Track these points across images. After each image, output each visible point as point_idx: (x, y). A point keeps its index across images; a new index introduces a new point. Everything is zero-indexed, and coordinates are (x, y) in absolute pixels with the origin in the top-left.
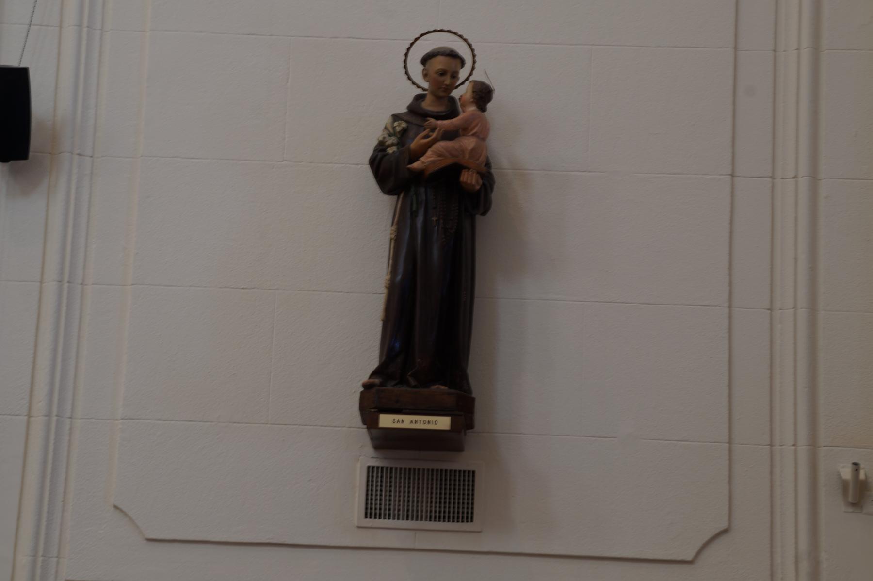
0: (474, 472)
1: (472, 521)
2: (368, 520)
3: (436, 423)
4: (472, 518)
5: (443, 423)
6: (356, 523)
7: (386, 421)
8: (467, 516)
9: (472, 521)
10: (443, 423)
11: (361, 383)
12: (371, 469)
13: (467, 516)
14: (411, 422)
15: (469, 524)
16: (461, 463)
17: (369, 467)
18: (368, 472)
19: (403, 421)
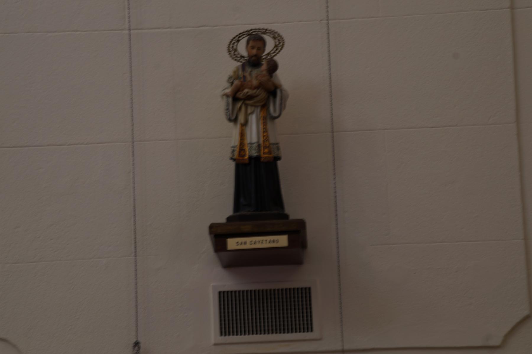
0: (310, 289)
1: (312, 331)
2: (223, 337)
3: (277, 241)
4: (312, 328)
5: (283, 241)
6: (213, 342)
7: (232, 243)
8: (308, 327)
9: (312, 331)
10: (283, 241)
11: (226, 78)
12: (225, 298)
13: (308, 327)
14: (270, 242)
15: (310, 333)
16: (297, 279)
17: (220, 293)
18: (220, 297)
19: (245, 243)
